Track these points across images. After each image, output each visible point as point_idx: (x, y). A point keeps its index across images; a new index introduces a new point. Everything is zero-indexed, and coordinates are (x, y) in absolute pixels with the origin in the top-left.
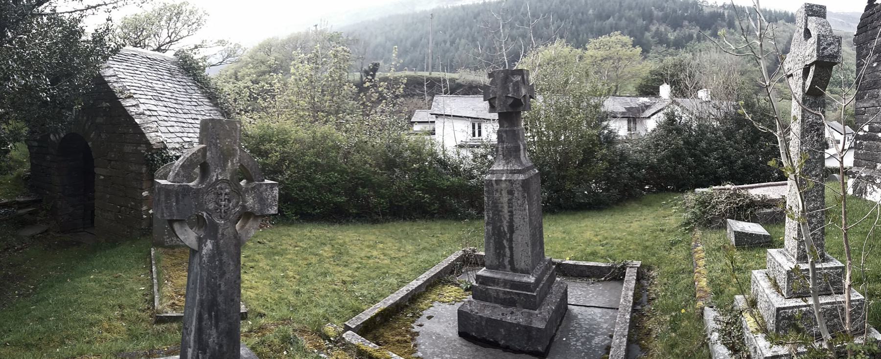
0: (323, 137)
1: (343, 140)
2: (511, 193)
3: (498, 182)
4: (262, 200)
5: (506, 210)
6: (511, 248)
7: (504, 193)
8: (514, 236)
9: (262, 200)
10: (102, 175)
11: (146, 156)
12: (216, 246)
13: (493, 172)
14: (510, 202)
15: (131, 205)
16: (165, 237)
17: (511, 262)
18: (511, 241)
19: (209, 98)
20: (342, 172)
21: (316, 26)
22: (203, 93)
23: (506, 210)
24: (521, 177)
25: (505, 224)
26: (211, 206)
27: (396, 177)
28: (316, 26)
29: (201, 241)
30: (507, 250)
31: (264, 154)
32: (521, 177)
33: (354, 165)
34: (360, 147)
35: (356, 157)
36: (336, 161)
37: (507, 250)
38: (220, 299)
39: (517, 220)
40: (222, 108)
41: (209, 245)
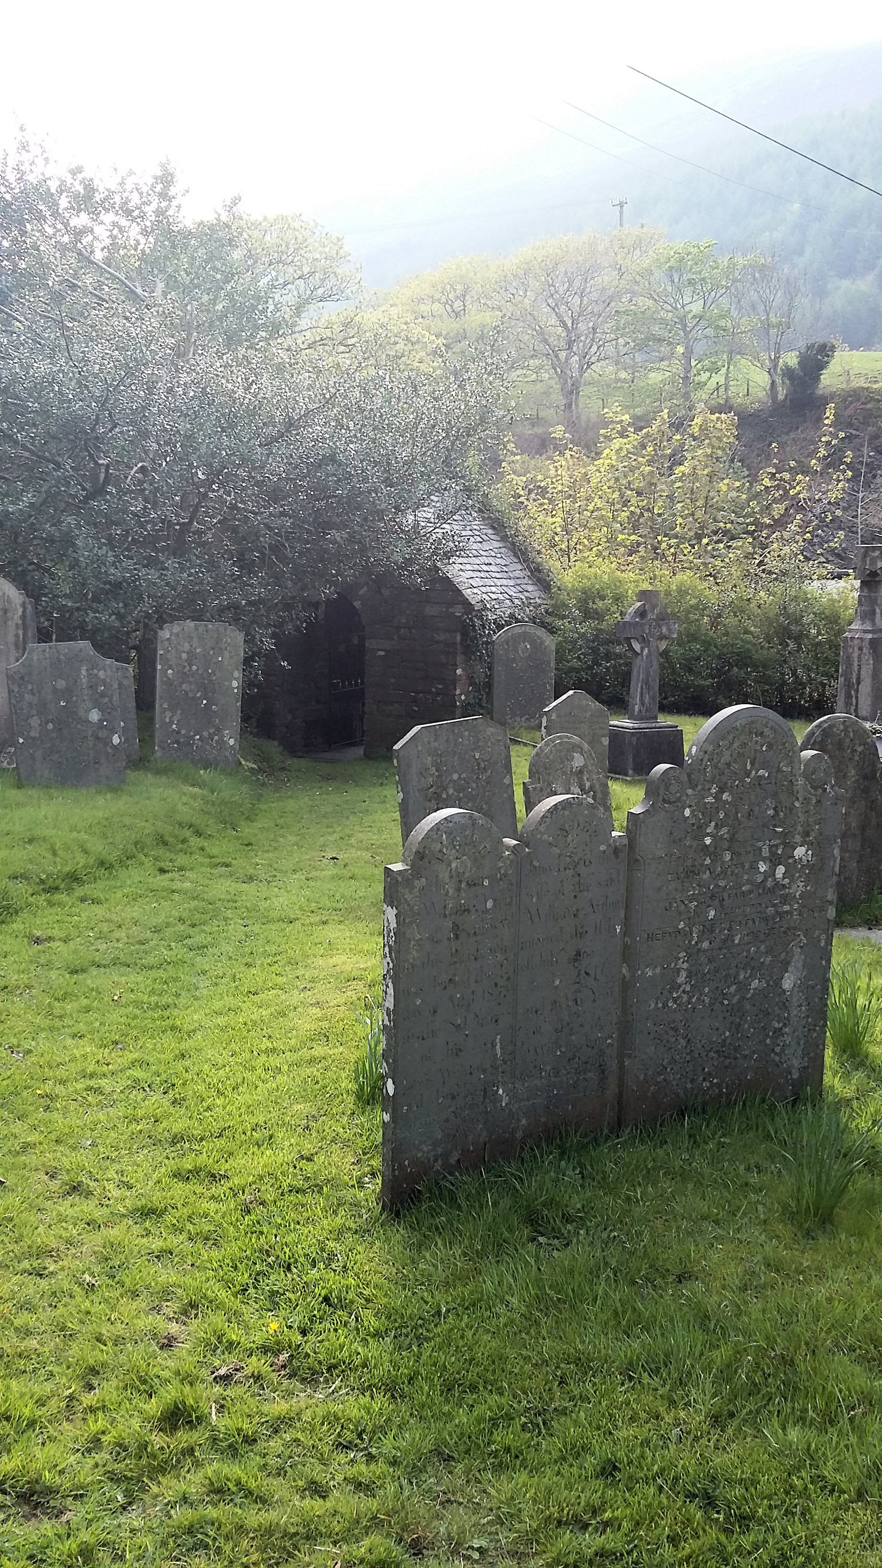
0: (679, 591)
1: (711, 597)
2: (860, 649)
3: (852, 638)
4: (669, 630)
5: (856, 663)
6: (857, 698)
7: (856, 649)
8: (860, 686)
9: (669, 630)
10: (382, 650)
11: (465, 620)
12: (649, 650)
13: (850, 631)
14: (859, 657)
15: (437, 688)
16: (507, 717)
17: (856, 710)
18: (857, 691)
19: (493, 528)
20: (708, 644)
21: (621, 205)
22: (484, 519)
23: (856, 663)
24: (870, 636)
25: (854, 676)
26: (647, 631)
27: (789, 653)
28: (621, 205)
29: (642, 649)
30: (854, 699)
31: (598, 616)
32: (870, 636)
33: (727, 634)
34: (739, 609)
35: (731, 621)
36: (699, 627)
37: (854, 699)
38: (650, 679)
39: (863, 673)
40: (513, 544)
41: (646, 651)
